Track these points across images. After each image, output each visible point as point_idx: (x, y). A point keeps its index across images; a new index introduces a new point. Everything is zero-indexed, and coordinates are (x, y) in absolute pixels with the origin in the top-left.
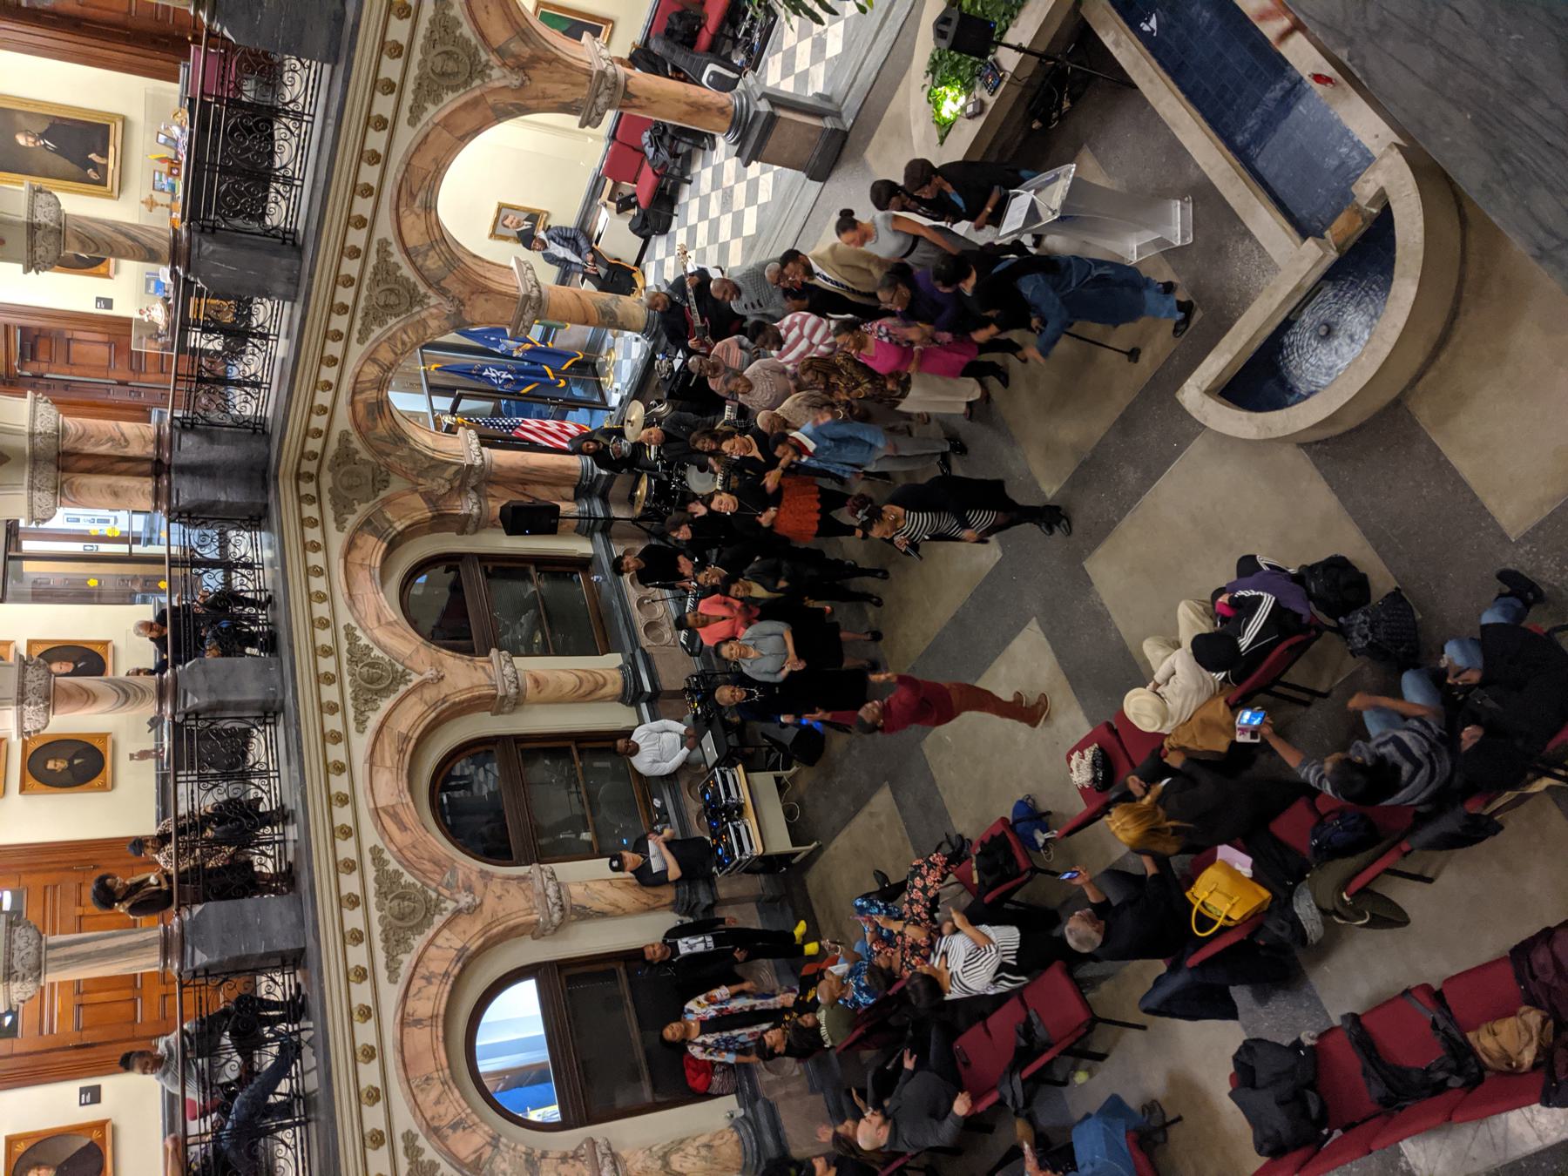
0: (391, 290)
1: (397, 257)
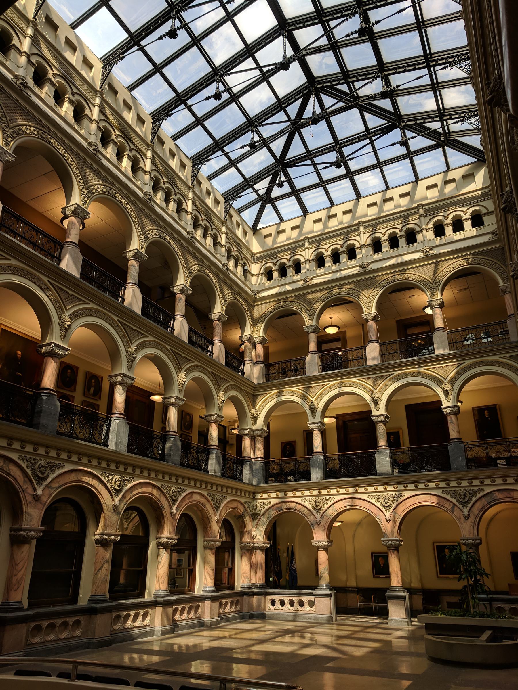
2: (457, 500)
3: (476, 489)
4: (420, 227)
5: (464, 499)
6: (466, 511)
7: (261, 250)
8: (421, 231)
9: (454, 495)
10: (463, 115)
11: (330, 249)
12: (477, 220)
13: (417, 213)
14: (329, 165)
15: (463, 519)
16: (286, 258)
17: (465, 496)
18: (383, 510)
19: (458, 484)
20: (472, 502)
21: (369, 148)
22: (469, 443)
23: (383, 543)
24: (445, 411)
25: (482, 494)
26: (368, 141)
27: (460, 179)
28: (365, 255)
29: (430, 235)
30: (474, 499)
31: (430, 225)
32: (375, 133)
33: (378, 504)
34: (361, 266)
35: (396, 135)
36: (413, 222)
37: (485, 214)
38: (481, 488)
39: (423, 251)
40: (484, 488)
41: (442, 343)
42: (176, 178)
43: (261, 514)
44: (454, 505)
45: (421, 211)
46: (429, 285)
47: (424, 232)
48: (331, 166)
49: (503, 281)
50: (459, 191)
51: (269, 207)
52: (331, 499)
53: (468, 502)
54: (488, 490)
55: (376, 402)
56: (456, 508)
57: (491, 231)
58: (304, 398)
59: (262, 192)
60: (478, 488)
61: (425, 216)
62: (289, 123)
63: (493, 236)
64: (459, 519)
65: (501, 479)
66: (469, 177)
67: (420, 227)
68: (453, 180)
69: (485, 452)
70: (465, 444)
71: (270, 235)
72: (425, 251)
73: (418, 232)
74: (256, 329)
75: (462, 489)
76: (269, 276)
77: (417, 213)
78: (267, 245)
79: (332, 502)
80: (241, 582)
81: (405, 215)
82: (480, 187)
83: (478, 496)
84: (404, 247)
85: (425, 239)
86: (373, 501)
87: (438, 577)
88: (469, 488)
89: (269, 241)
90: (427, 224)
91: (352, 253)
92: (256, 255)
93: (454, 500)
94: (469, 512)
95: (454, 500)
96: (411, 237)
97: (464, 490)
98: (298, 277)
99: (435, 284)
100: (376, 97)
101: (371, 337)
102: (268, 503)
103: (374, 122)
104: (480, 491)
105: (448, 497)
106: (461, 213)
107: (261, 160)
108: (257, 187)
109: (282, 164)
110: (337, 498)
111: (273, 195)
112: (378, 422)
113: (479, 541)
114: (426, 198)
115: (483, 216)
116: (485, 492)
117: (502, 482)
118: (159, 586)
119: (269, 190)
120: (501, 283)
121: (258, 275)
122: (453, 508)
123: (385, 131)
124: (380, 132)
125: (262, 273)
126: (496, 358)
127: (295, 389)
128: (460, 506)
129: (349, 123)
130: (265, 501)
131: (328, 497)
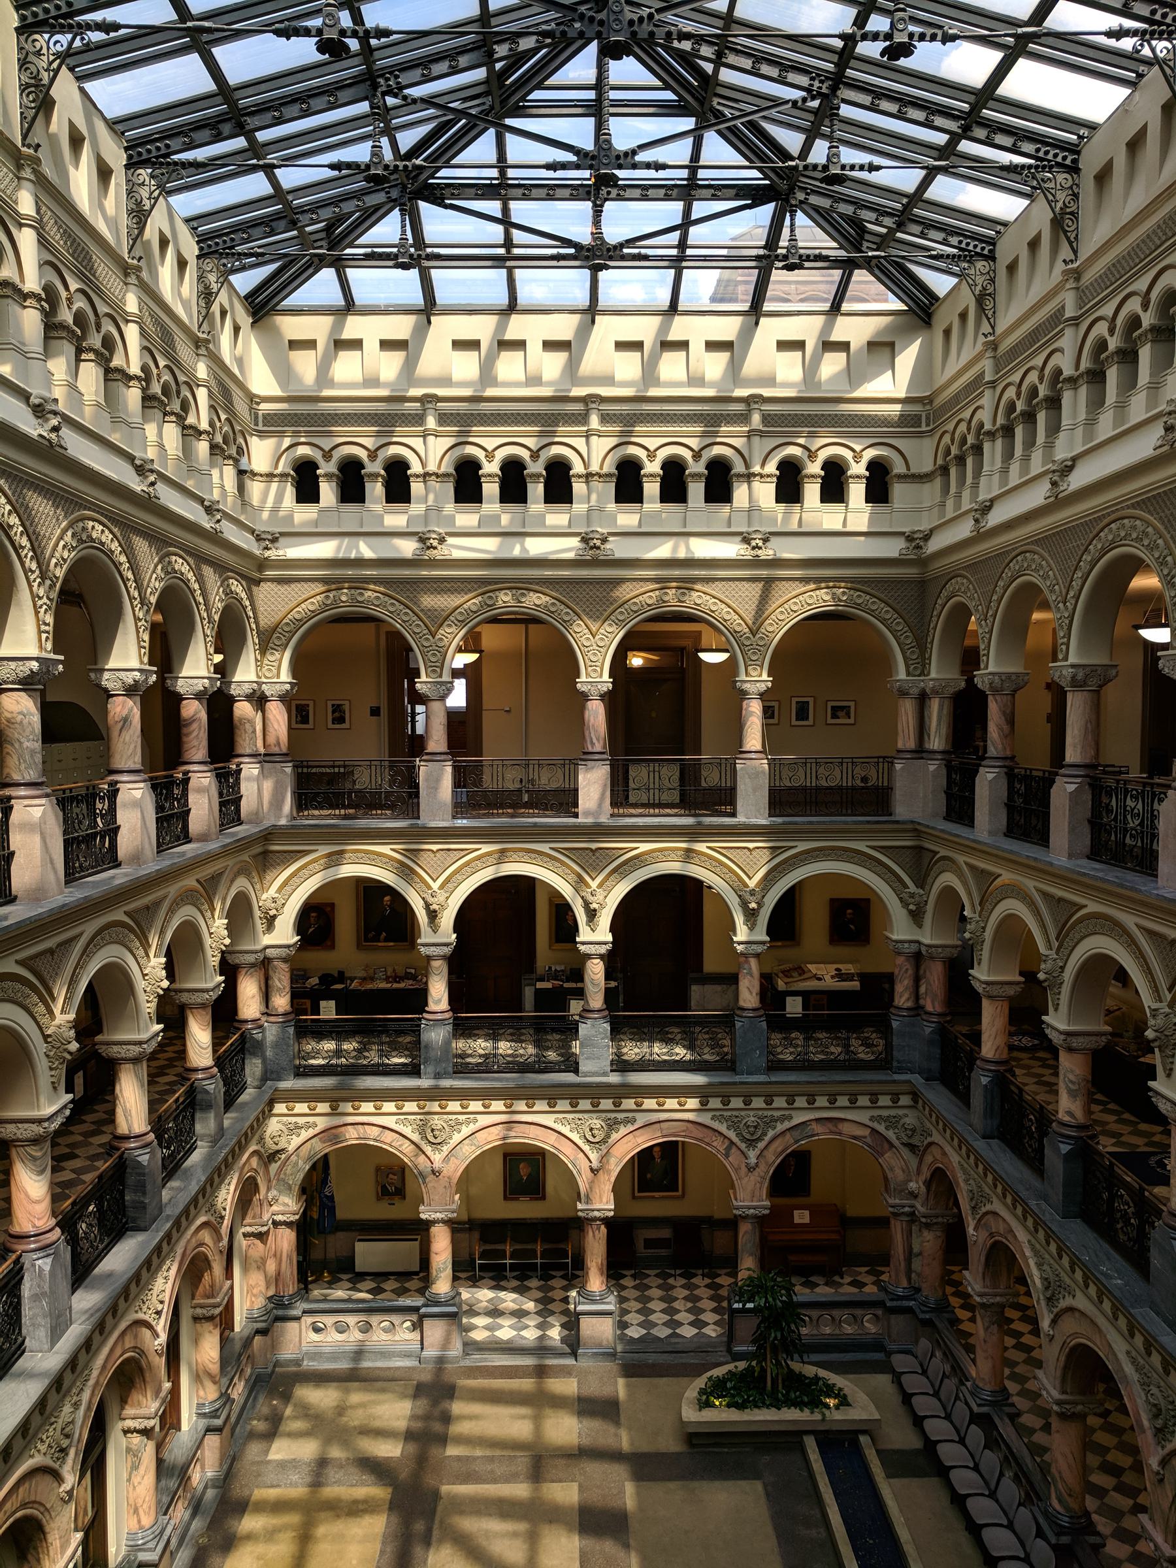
3: (777, 1114)
4: (747, 466)
6: (752, 1155)
7: (278, 392)
8: (749, 477)
9: (734, 1124)
11: (501, 454)
12: (879, 485)
13: (744, 418)
15: (744, 1170)
16: (359, 443)
18: (586, 1148)
20: (767, 1139)
24: (740, 948)
25: (787, 1125)
27: (861, 349)
28: (592, 498)
29: (765, 492)
30: (771, 1133)
31: (771, 468)
32: (717, 191)
33: (575, 1137)
34: (585, 540)
36: (730, 442)
37: (902, 478)
39: (746, 540)
40: (793, 1113)
41: (755, 790)
42: (94, 248)
44: (732, 1143)
45: (756, 418)
47: (756, 484)
49: (907, 666)
50: (853, 390)
52: (468, 1122)
53: (759, 1139)
55: (592, 915)
56: (734, 1149)
57: (907, 529)
58: (406, 872)
61: (761, 434)
62: (509, 122)
64: (737, 1170)
66: (882, 349)
67: (747, 466)
68: (844, 346)
71: (311, 344)
72: (753, 543)
73: (739, 475)
74: (272, 657)
76: (307, 492)
77: (744, 418)
78: (299, 380)
79: (473, 1127)
80: (247, 1305)
81: (713, 414)
82: (902, 395)
83: (780, 1127)
85: (753, 509)
86: (565, 1130)
87: (634, 1197)
89: (305, 365)
90: (763, 465)
92: (263, 406)
93: (732, 1135)
95: (732, 1135)
96: (720, 482)
98: (396, 519)
101: (593, 744)
102: (308, 1126)
104: (783, 1119)
105: (723, 1128)
106: (848, 454)
110: (484, 1120)
112: (588, 956)
114: (771, 381)
118: (139, 1521)
120: (902, 675)
121: (270, 476)
122: (728, 1149)
125: (284, 475)
127: (385, 849)
128: (743, 1146)
130: (301, 1120)
131: (462, 1118)
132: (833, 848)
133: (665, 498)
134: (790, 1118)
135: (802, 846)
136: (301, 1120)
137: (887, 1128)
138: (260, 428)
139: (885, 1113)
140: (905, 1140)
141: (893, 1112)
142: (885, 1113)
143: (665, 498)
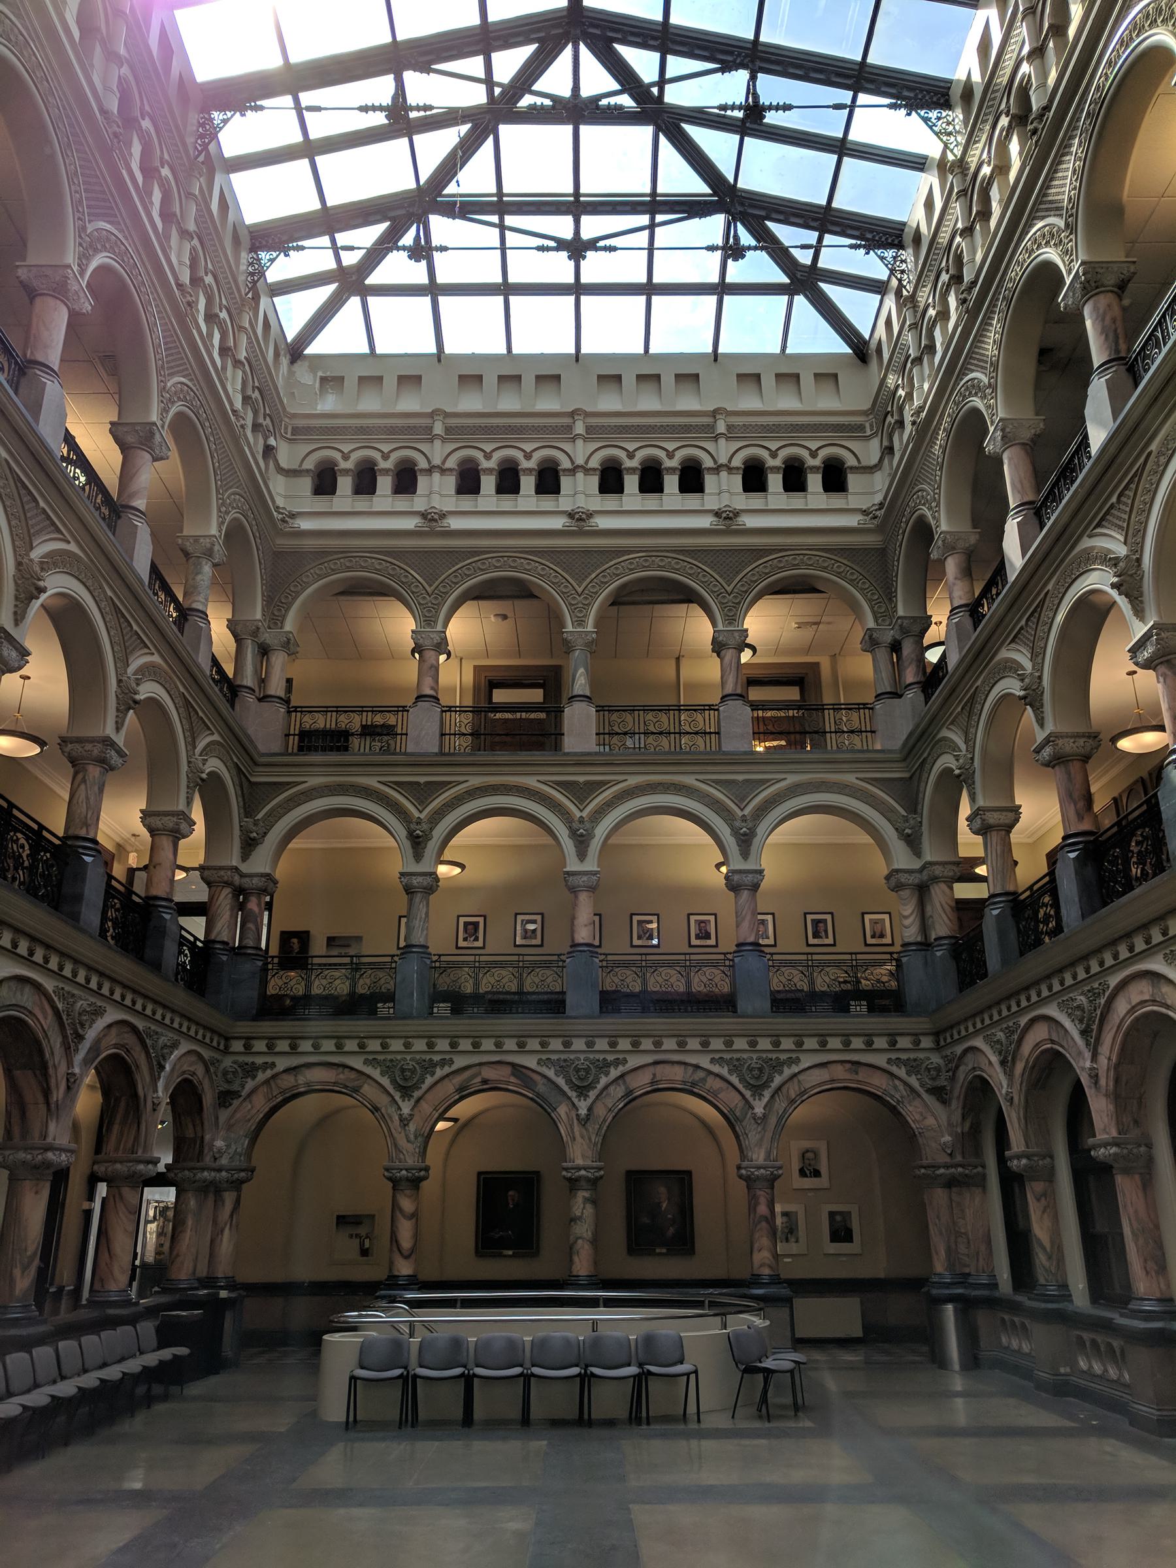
0: (587, 1070)
1: (614, 1073)
2: (569, 1082)
5: (757, 1078)
10: (869, 236)
14: (601, 244)
17: (587, 1073)
19: (519, 1047)
20: (600, 1086)
21: (642, 238)
22: (443, 959)
23: (564, 1173)
26: (644, 220)
30: (429, 1080)
35: (713, 227)
38: (794, 1056)
43: (244, 1093)
46: (574, 598)
48: (557, 249)
49: (874, 613)
51: (354, 303)
54: (460, 1062)
59: (350, 259)
60: (789, 1055)
63: (868, 518)
65: (746, 1039)
69: (515, 982)
70: (603, 957)
72: (724, 515)
73: (709, 469)
75: (755, 1056)
83: (439, 1073)
84: (489, 496)
88: (770, 1056)
91: (406, 480)
94: (412, 1109)
97: (758, 1059)
99: (586, 598)
100: (701, 117)
103: (680, 178)
104: (443, 1063)
107: (386, 170)
108: (342, 238)
109: (428, 199)
111: (376, 278)
113: (422, 1173)
115: (521, 473)
116: (454, 1067)
117: (676, 1047)
119: (375, 256)
123: (690, 208)
124: (685, 208)
126: (851, 778)
128: (573, 1094)
129: (621, 157)
132: (289, 799)
133: (500, 490)
134: (797, 1061)
135: (791, 779)
136: (259, 1060)
137: (908, 1073)
138: (289, 436)
139: (904, 1056)
140: (930, 1083)
141: (912, 1056)
142: (904, 1056)
143: (500, 490)
